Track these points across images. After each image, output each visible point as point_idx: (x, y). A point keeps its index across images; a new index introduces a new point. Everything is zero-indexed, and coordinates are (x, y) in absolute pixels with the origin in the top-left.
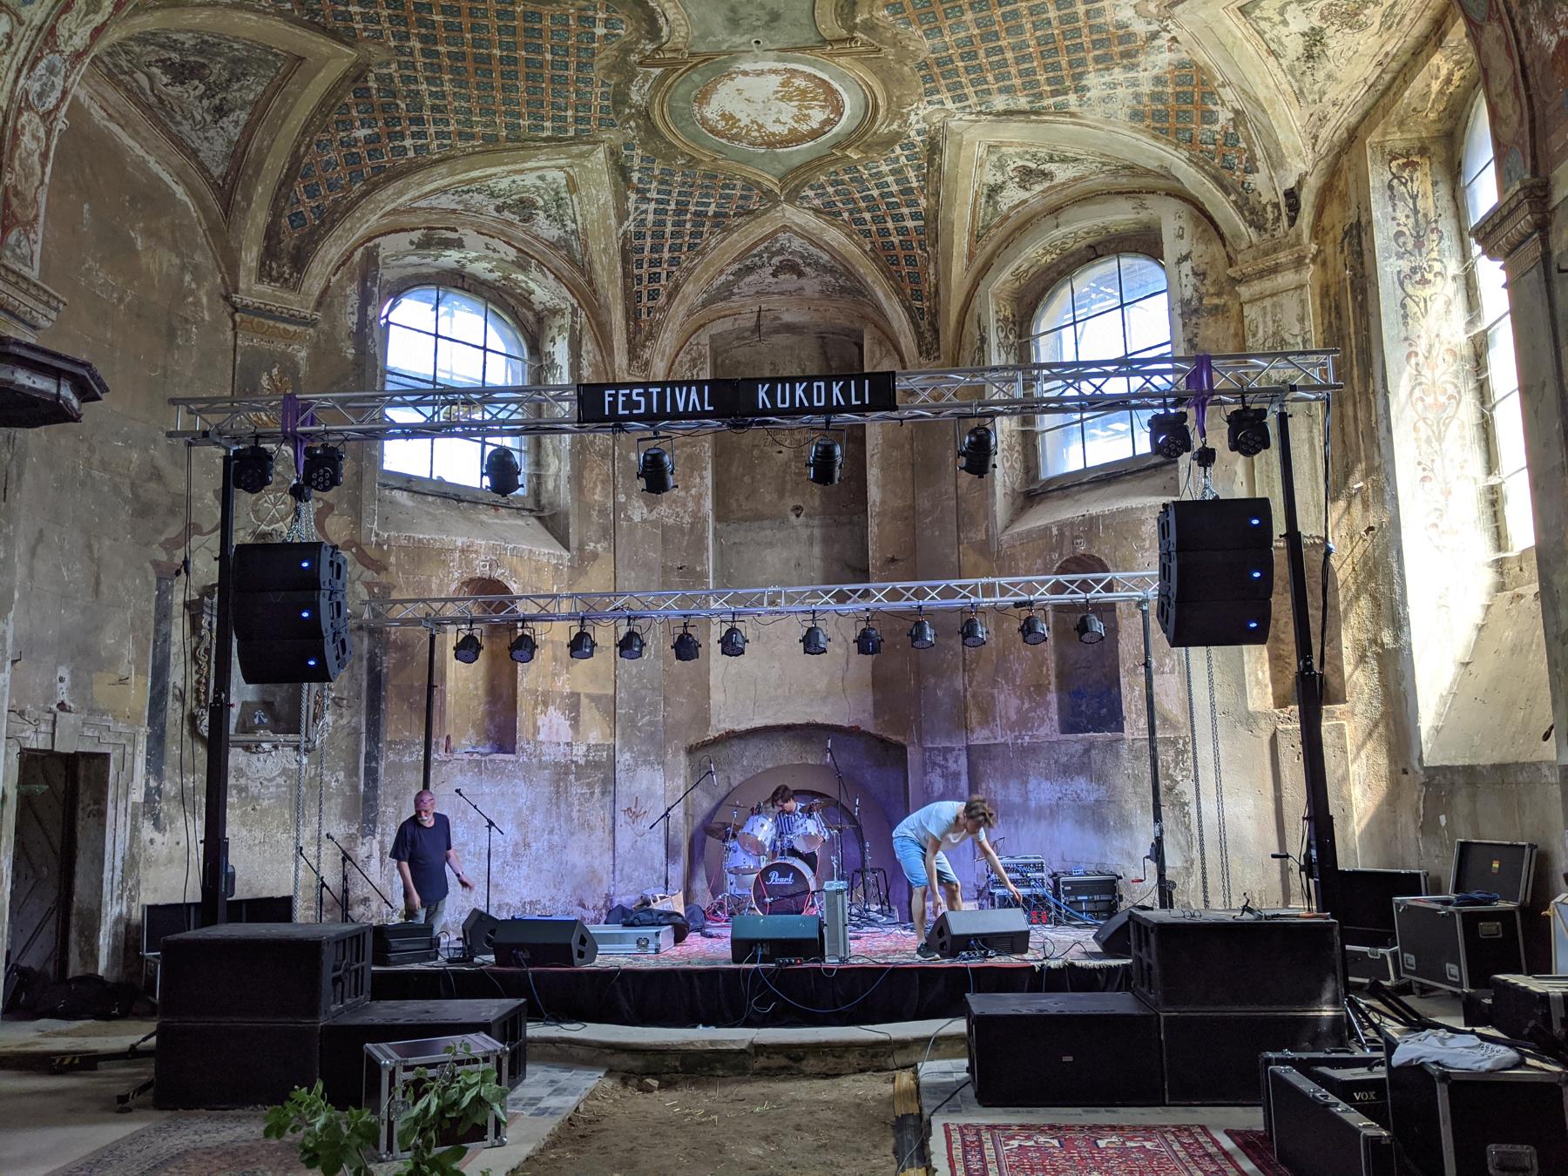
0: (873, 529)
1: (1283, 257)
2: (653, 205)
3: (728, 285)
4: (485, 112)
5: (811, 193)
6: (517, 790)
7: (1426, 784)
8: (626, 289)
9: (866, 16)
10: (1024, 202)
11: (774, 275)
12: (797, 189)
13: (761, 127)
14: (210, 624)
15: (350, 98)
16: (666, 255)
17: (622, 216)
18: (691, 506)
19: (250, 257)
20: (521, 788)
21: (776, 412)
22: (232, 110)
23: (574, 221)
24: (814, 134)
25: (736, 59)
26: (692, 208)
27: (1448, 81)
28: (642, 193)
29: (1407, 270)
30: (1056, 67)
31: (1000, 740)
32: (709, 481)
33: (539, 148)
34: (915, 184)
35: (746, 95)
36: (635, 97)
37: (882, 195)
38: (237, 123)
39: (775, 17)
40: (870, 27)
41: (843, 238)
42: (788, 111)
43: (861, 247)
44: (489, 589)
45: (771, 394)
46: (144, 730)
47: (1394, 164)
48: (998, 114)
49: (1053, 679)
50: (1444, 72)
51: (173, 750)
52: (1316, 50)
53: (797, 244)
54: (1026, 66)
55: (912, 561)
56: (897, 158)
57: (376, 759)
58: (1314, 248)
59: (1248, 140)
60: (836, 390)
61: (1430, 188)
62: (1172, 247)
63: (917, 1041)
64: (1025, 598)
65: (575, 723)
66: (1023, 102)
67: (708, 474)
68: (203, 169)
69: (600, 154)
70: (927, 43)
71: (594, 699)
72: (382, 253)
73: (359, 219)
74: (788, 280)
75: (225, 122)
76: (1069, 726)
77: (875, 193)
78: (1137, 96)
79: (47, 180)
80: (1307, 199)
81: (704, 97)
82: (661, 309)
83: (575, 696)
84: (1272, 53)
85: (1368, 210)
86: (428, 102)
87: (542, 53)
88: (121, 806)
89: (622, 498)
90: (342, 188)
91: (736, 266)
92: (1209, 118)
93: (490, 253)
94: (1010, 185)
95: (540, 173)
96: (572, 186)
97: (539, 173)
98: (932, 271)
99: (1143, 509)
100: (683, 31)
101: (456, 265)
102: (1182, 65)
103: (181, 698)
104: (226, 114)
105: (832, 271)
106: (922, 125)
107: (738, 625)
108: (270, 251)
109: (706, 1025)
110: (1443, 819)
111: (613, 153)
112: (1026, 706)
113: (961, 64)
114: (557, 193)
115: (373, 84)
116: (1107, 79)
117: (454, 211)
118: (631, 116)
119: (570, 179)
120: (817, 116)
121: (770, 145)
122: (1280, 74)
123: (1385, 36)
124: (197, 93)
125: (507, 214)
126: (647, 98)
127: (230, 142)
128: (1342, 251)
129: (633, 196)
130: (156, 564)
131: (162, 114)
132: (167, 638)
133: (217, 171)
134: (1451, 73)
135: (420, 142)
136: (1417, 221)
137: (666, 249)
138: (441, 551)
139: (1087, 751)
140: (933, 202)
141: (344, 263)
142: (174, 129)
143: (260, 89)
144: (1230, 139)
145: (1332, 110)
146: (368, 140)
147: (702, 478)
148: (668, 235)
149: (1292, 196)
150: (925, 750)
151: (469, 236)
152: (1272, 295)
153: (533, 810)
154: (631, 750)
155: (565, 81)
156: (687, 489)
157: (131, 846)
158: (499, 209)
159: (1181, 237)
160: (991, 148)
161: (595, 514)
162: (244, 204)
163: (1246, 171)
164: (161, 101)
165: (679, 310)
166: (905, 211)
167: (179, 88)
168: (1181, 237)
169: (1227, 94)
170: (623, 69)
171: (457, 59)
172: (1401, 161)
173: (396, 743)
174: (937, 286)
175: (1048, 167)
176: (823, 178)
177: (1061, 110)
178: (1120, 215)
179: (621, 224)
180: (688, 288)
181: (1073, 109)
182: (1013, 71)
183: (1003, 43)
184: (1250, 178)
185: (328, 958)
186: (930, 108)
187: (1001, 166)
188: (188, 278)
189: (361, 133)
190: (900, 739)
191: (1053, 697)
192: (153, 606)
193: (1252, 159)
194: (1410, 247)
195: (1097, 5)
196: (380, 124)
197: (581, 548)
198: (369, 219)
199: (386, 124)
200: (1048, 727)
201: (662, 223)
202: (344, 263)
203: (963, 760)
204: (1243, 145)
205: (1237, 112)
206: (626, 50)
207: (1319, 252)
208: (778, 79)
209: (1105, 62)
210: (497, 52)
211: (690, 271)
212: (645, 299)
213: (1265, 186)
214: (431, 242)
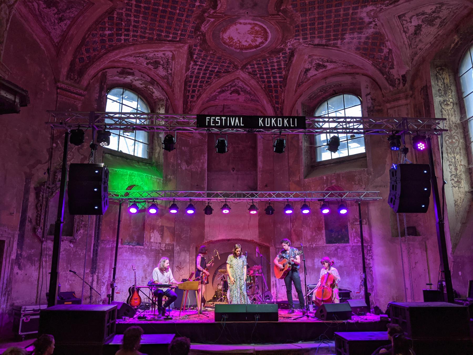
0: (259, 176)
1: (402, 95)
2: (198, 67)
3: (216, 96)
4: (152, 29)
5: (249, 67)
6: (144, 258)
8: (184, 94)
9: (284, 7)
10: (316, 75)
11: (231, 94)
12: (246, 65)
13: (240, 42)
14: (43, 195)
15: (106, 20)
16: (199, 84)
17: (187, 69)
18: (201, 166)
19: (64, 71)
20: (145, 258)
21: (265, 127)
22: (65, 20)
23: (171, 70)
24: (257, 46)
25: (239, 18)
26: (210, 69)
27: (457, 44)
28: (195, 62)
29: (442, 101)
30: (338, 31)
32: (206, 158)
33: (166, 44)
34: (283, 67)
35: (239, 31)
36: (203, 28)
37: (271, 70)
38: (66, 24)
39: (256, 5)
40: (285, 11)
41: (256, 83)
42: (251, 37)
43: (261, 86)
44: (233, 171)
45: (264, 121)
46: (17, 232)
47: (437, 69)
48: (315, 45)
49: (324, 225)
50: (456, 41)
51: (27, 241)
52: (418, 32)
53: (240, 84)
54: (329, 29)
55: (271, 185)
56: (280, 57)
57: (97, 246)
58: (411, 92)
59: (392, 59)
60: (285, 121)
61: (448, 77)
62: (364, 91)
63: (312, 349)
64: (322, 198)
65: (162, 237)
66: (324, 42)
67: (206, 155)
68: (51, 39)
69: (186, 47)
70: (301, 18)
72: (108, 74)
73: (102, 62)
74: (235, 96)
75: (62, 24)
76: (329, 241)
77: (270, 68)
78: (359, 43)
79: (7, 29)
80: (409, 79)
81: (225, 31)
82: (195, 102)
83: (162, 226)
84: (404, 31)
85: (430, 82)
86: (133, 24)
87: (176, 10)
88: (8, 260)
89: (179, 162)
90: (98, 50)
91: (219, 90)
92: (381, 51)
93: (142, 78)
94: (312, 69)
95: (164, 52)
96: (173, 58)
97: (164, 52)
98: (283, 95)
99: (355, 172)
100: (225, 6)
101: (130, 81)
102: (376, 33)
103: (30, 221)
104: (63, 21)
105: (250, 94)
106: (291, 47)
107: (227, 203)
108: (71, 70)
109: (255, 343)
110: (460, 273)
111: (190, 48)
112: (314, 234)
113: (309, 27)
114: (168, 60)
115: (115, 16)
116: (352, 36)
117: (132, 63)
118: (199, 35)
119: (173, 55)
120: (259, 40)
121: (242, 49)
122: (405, 38)
123: (440, 29)
124: (54, 12)
125: (150, 66)
126: (206, 29)
127: (62, 31)
128: (421, 94)
129: (192, 63)
130: (25, 173)
131: (40, 19)
132: (27, 200)
133: (56, 41)
134: (458, 42)
135: (126, 38)
136: (444, 86)
137: (199, 82)
138: (122, 175)
139: (336, 250)
140: (287, 73)
141: (95, 76)
142: (43, 24)
143: (76, 13)
144: (386, 58)
145: (419, 51)
146: (110, 35)
147: (204, 157)
148: (200, 77)
149: (404, 76)
150: (276, 248)
151: (136, 72)
152: (397, 107)
153: (148, 266)
154: (179, 246)
155: (180, 20)
156: (199, 160)
157: (10, 275)
158: (147, 64)
159: (367, 88)
160: (310, 56)
161: (171, 166)
162: (64, 53)
163: (390, 68)
164: (41, 14)
165: (200, 102)
166: (278, 75)
167: (48, 10)
168: (367, 88)
169: (388, 44)
170: (201, 19)
171: (146, 9)
172: (439, 68)
173: (104, 241)
174: (284, 100)
175: (326, 64)
176: (255, 62)
177: (335, 45)
178: (347, 80)
179: (186, 72)
180: (204, 96)
181: (338, 45)
182: (324, 30)
183: (324, 21)
184: (391, 70)
185: (107, 317)
186: (295, 41)
187: (311, 63)
188: (43, 75)
189: (107, 32)
190: (268, 244)
191: (324, 231)
192: (23, 188)
193: (393, 65)
194: (443, 94)
195: (356, 11)
196: (115, 30)
198: (105, 62)
199: (117, 30)
200: (322, 242)
201: (199, 73)
202: (95, 76)
204: (390, 60)
205: (390, 49)
206: (204, 11)
207: (413, 94)
208: (250, 26)
209: (353, 31)
210: (161, 8)
211: (205, 90)
212: (190, 98)
213: (396, 73)
214: (124, 72)
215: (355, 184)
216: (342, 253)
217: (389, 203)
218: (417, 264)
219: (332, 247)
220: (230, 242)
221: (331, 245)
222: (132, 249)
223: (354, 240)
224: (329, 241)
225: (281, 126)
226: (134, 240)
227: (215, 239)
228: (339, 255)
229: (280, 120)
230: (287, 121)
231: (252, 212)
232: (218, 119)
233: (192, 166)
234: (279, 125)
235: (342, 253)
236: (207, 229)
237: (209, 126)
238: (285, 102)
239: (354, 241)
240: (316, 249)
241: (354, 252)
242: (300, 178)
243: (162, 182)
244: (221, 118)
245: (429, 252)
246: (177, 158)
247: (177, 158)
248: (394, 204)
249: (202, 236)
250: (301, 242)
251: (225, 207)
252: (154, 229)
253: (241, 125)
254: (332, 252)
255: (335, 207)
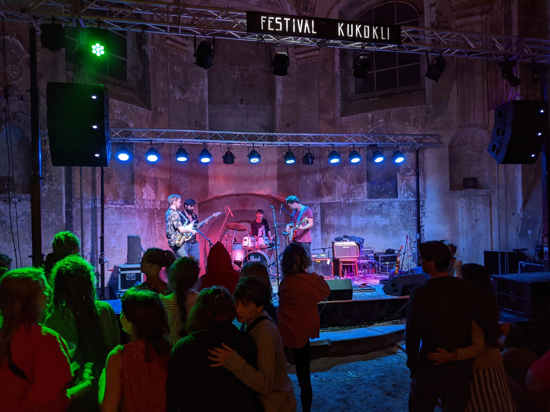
0: (278, 111)
6: (136, 221)
7: (523, 219)
20: (137, 220)
31: (337, 201)
32: (206, 83)
44: (241, 104)
45: (344, 28)
49: (365, 177)
65: (156, 192)
67: (206, 80)
71: (163, 180)
83: (156, 178)
110: (530, 232)
112: (352, 187)
128: (501, 10)
139: (380, 206)
147: (204, 82)
156: (197, 86)
161: (160, 93)
174: (315, 5)
191: (365, 184)
197: (156, 109)
203: (319, 209)
215: (410, 125)
216: (388, 210)
217: (489, 151)
218: (478, 222)
219: (376, 202)
220: (239, 197)
221: (374, 200)
222: (120, 209)
223: (404, 194)
224: (371, 196)
225: (368, 37)
226: (119, 197)
227: (223, 194)
228: (385, 212)
229: (367, 28)
230: (377, 31)
231: (289, 162)
232: (278, 20)
233: (188, 95)
234: (365, 37)
235: (388, 210)
236: (211, 182)
237: (266, 31)
238: (317, 9)
239: (405, 195)
240: (354, 205)
241: (403, 208)
242: (334, 116)
243: (151, 116)
244: (283, 19)
245: (495, 208)
246: (168, 82)
247: (168, 82)
248: (497, 153)
249: (205, 191)
250: (333, 197)
251: (253, 154)
252: (145, 182)
253: (313, 32)
254: (374, 209)
255: (389, 153)
